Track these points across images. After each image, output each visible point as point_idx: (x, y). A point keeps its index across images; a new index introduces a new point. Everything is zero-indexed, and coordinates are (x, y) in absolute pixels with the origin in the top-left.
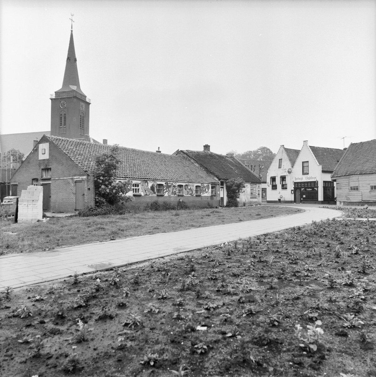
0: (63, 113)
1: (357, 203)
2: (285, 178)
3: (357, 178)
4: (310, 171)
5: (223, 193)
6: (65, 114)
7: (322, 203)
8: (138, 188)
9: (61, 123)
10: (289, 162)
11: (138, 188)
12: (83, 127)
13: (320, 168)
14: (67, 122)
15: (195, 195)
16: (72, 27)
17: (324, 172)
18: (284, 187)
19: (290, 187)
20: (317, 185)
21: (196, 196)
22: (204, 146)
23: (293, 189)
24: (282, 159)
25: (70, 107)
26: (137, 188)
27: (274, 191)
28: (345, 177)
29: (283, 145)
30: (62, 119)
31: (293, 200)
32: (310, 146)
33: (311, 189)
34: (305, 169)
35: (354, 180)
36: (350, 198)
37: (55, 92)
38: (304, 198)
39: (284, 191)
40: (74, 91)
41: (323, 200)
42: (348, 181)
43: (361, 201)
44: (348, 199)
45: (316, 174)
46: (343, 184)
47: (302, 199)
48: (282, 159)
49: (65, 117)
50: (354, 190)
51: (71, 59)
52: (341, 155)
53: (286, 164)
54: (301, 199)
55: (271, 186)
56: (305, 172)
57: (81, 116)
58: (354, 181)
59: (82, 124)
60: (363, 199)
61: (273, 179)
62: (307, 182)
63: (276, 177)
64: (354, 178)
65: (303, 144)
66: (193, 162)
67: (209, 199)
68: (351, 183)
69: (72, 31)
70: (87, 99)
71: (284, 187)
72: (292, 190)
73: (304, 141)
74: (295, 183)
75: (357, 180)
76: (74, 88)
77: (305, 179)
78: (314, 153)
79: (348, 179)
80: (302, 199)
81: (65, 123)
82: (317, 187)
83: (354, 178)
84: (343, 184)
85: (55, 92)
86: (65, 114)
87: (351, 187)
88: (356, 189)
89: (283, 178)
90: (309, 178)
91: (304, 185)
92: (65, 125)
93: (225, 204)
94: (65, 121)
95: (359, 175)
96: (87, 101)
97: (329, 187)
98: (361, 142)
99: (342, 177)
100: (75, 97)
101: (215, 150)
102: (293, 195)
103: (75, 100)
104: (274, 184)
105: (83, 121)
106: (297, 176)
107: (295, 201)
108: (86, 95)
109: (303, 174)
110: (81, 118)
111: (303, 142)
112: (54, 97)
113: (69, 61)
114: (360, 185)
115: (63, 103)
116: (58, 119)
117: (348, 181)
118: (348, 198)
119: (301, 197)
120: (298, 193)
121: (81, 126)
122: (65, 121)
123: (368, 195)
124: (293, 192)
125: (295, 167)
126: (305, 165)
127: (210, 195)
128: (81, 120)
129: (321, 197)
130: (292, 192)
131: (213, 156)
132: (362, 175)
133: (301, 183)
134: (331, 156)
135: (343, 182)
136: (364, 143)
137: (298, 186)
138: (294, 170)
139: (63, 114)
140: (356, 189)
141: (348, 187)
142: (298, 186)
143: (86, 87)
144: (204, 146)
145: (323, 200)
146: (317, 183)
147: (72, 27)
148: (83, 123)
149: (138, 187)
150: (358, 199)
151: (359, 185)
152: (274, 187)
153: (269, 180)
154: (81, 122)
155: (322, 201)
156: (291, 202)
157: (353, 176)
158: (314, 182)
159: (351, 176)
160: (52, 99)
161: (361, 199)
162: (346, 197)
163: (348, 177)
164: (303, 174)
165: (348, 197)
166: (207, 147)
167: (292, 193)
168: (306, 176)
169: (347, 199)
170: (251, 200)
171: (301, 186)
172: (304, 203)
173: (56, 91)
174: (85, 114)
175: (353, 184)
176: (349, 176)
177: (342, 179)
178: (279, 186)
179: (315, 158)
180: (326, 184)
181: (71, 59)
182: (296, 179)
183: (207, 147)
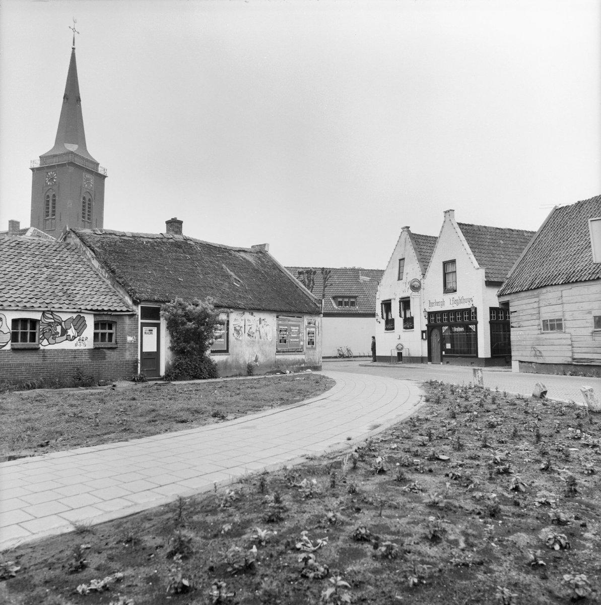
0: (51, 194)
1: (562, 368)
2: (390, 304)
3: (559, 294)
4: (460, 286)
5: (155, 341)
6: (54, 196)
7: (488, 362)
8: (111, 331)
9: (48, 212)
10: (418, 265)
11: (111, 331)
12: (89, 219)
13: (480, 275)
14: (57, 210)
15: (8, 347)
16: (74, 42)
17: (489, 284)
18: (409, 323)
19: (421, 323)
20: (476, 318)
21: (14, 350)
22: (168, 223)
23: (425, 328)
24: (404, 259)
25: (68, 180)
26: (107, 331)
27: (390, 334)
28: (530, 293)
29: (408, 228)
30: (49, 205)
31: (426, 354)
32: (460, 224)
33: (462, 329)
34: (450, 278)
35: (553, 302)
36: (544, 354)
37: (40, 157)
38: (447, 351)
39: (409, 334)
40: (72, 153)
41: (489, 356)
42: (536, 305)
43: (570, 360)
44: (539, 354)
45: (475, 293)
46: (525, 313)
47: (444, 353)
48: (404, 259)
49: (54, 200)
50: (552, 329)
51: (72, 97)
52: (526, 241)
53: (413, 270)
54: (442, 353)
55: (383, 322)
56: (449, 286)
57: (84, 198)
58: (550, 305)
59: (87, 213)
60: (576, 356)
61: (387, 305)
62: (455, 312)
63: (392, 301)
64: (550, 295)
65: (443, 219)
66: (90, 256)
67: (85, 359)
68: (543, 310)
69: (73, 49)
70: (100, 169)
71: (409, 323)
72: (423, 332)
73: (446, 212)
74: (430, 314)
75: (560, 302)
76: (73, 148)
77: (448, 303)
78: (467, 240)
79: (537, 300)
80: (444, 353)
81: (54, 211)
82: (476, 324)
83: (550, 294)
84: (525, 313)
85: (40, 157)
86: (54, 196)
87: (544, 321)
88: (555, 325)
89: (406, 303)
90: (456, 302)
91: (448, 319)
92: (54, 215)
93: (162, 372)
94: (54, 207)
95: (563, 288)
96: (101, 171)
97: (501, 320)
98: (579, 202)
99: (523, 294)
100: (72, 164)
101: (195, 230)
102: (426, 343)
103: (71, 169)
104: (408, 315)
105: (89, 208)
106: (433, 298)
107: (430, 358)
108: (98, 161)
109: (447, 290)
110: (84, 202)
111: (443, 214)
112: (37, 165)
113: (66, 101)
114: (567, 316)
115: (52, 175)
116: (42, 205)
117: (536, 305)
118: (538, 353)
119: (443, 348)
120: (436, 339)
121: (83, 217)
122: (54, 207)
123: (587, 346)
124: (424, 337)
125: (428, 274)
126: (450, 269)
127: (90, 344)
128: (84, 206)
129: (484, 349)
130: (424, 334)
131: (186, 246)
132: (569, 286)
133: (441, 313)
134: (518, 247)
135: (524, 307)
136: (585, 202)
137: (435, 320)
138: (426, 283)
139: (51, 196)
140: (555, 325)
141: (537, 322)
142: (436, 320)
143: (97, 147)
144: (168, 223)
145: (489, 356)
146: (476, 312)
147: (74, 42)
148: (89, 212)
149: (110, 328)
150: (561, 355)
151: (563, 316)
152: (390, 325)
153: (378, 310)
154: (84, 210)
155: (486, 359)
156: (421, 360)
157: (549, 289)
158: (469, 310)
159: (544, 290)
160: (33, 169)
161: (570, 354)
162: (533, 348)
163: (536, 292)
164: (447, 290)
165: (540, 348)
166: (175, 225)
167: (422, 338)
168: (451, 296)
169: (535, 356)
170: (280, 357)
171: (441, 320)
172: (448, 363)
173: (42, 153)
174: (93, 196)
175: (548, 314)
176: (539, 291)
177: (523, 298)
178: (399, 322)
179: (469, 251)
180: (498, 317)
181: (72, 97)
182: (431, 304)
183: (175, 225)
